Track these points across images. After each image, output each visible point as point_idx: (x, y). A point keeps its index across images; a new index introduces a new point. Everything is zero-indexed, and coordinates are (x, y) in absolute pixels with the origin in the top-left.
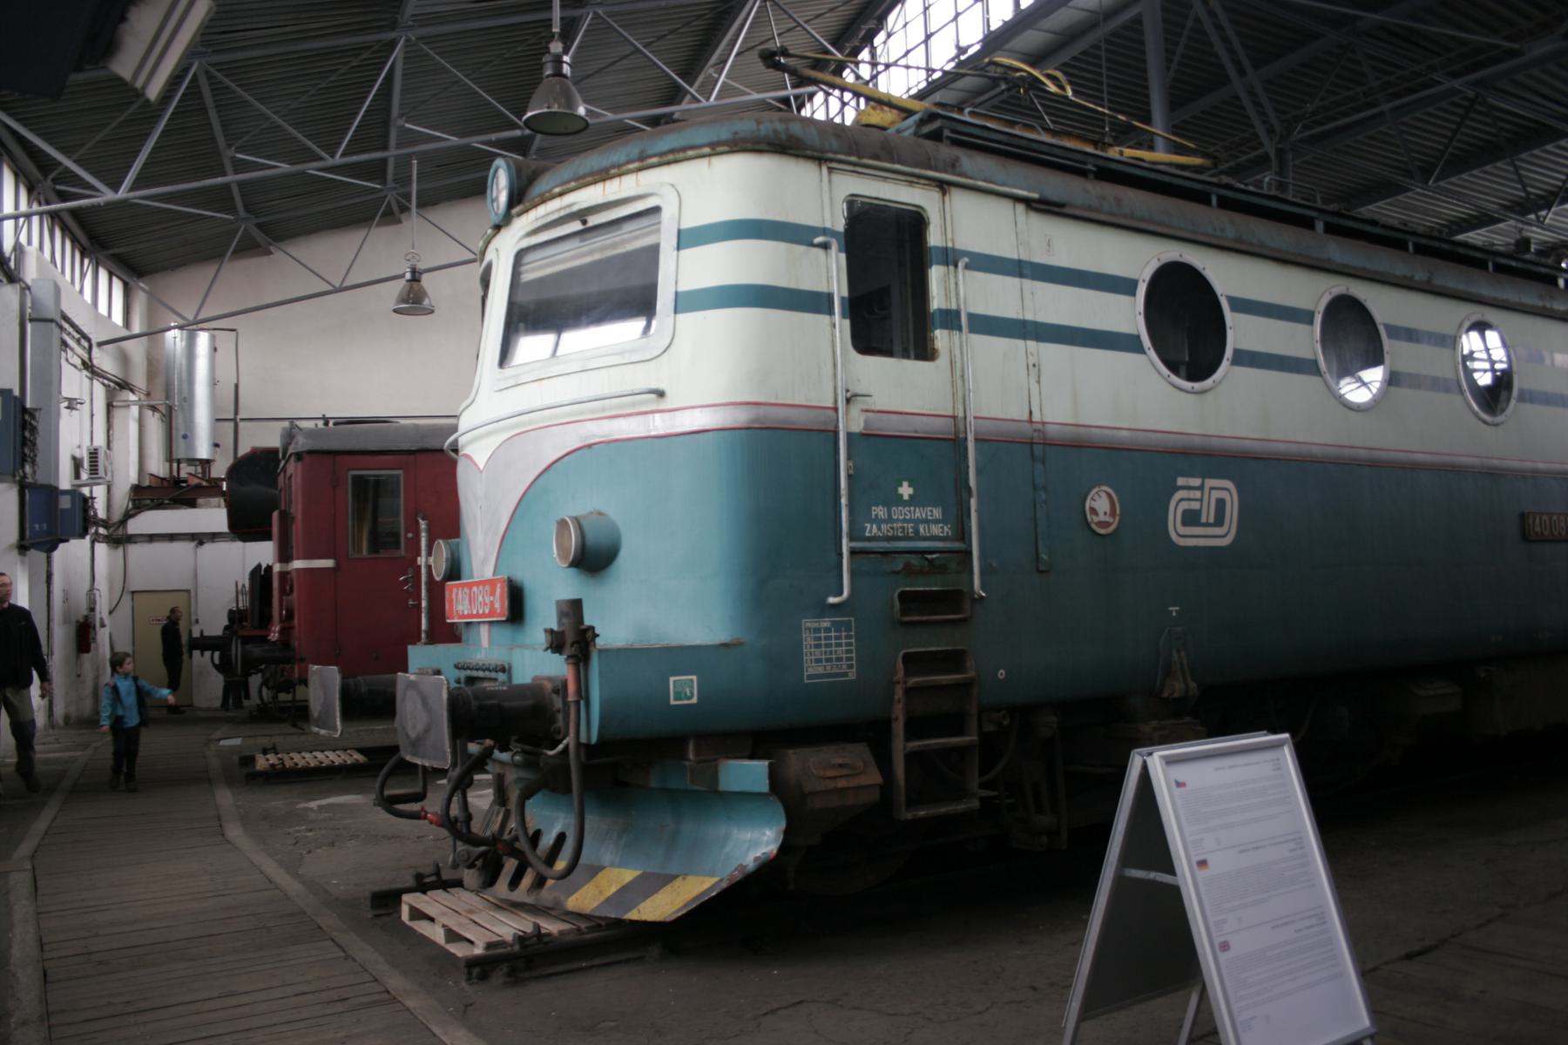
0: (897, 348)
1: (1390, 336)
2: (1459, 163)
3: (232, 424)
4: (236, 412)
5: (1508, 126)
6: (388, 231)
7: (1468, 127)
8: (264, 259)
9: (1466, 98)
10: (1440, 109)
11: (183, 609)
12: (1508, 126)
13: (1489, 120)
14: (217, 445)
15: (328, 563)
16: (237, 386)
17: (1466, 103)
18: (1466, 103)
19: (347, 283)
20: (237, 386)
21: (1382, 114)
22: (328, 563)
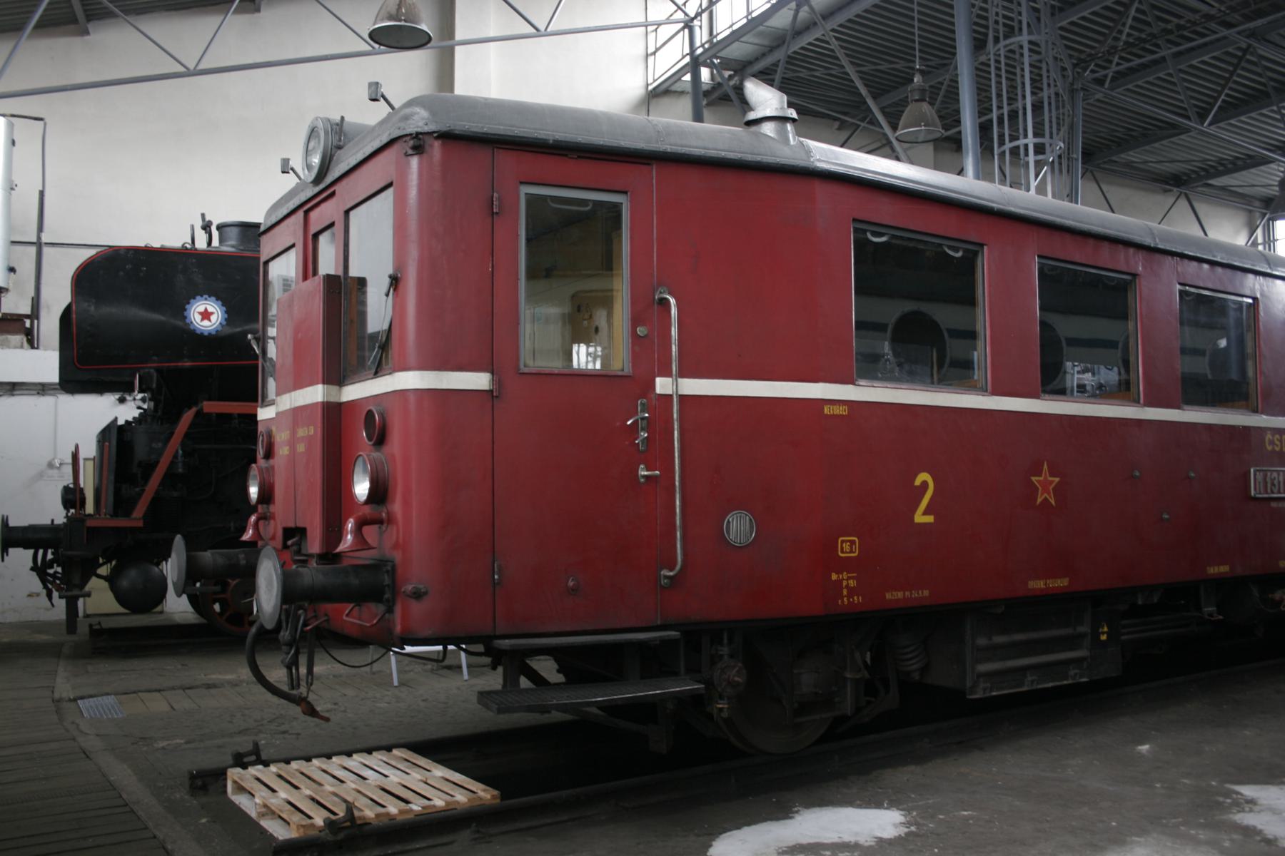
0: (412, 397)
1: (951, 336)
2: (1233, 108)
3: (33, 249)
4: (40, 228)
5: (1275, 76)
6: (244, 19)
7: (1239, 76)
8: (77, 41)
9: (1239, 49)
10: (1148, 82)
11: (1256, 808)
12: (1275, 76)
13: (1259, 70)
14: (12, 270)
15: (478, 381)
16: (42, 194)
17: (1240, 54)
18: (1240, 54)
19: (202, 66)
20: (42, 194)
21: (1163, 58)
22: (478, 381)
